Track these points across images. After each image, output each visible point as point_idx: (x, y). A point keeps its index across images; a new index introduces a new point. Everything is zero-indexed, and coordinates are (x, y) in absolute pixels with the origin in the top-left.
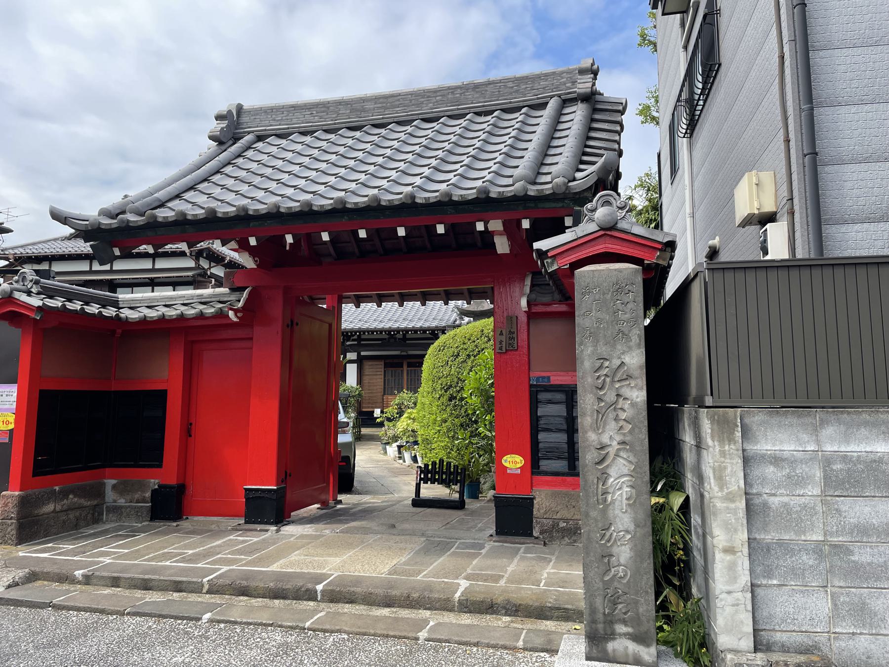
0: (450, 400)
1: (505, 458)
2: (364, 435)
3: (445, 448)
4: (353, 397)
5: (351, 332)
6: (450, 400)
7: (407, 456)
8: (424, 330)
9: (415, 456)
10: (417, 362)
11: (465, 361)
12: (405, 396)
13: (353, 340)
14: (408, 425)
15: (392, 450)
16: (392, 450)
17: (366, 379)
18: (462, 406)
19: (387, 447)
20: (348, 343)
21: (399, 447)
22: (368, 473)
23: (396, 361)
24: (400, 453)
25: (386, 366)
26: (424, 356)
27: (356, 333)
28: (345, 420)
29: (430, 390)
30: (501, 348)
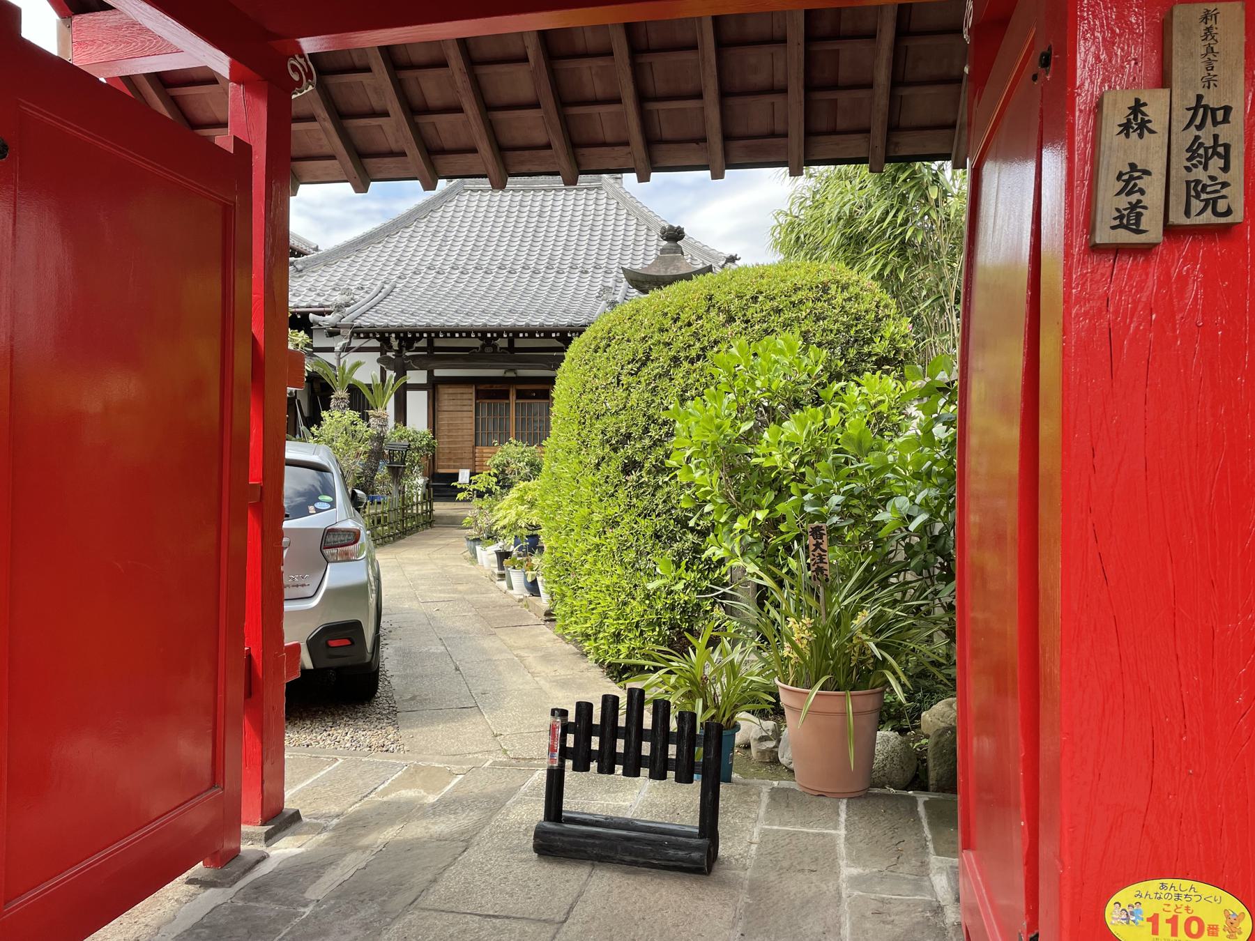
0: (626, 470)
1: (1125, 896)
2: (441, 517)
3: (612, 590)
4: (418, 449)
5: (413, 333)
6: (626, 470)
7: (516, 577)
8: (547, 333)
9: (534, 582)
10: (542, 390)
11: (666, 374)
12: (512, 452)
13: (418, 349)
14: (519, 515)
15: (486, 555)
16: (486, 555)
17: (443, 419)
18: (657, 487)
19: (478, 548)
20: (408, 354)
21: (503, 556)
22: (431, 619)
23: (496, 387)
24: (501, 567)
25: (480, 395)
26: (551, 381)
27: (421, 333)
28: (350, 525)
29: (574, 444)
30: (1130, 218)
